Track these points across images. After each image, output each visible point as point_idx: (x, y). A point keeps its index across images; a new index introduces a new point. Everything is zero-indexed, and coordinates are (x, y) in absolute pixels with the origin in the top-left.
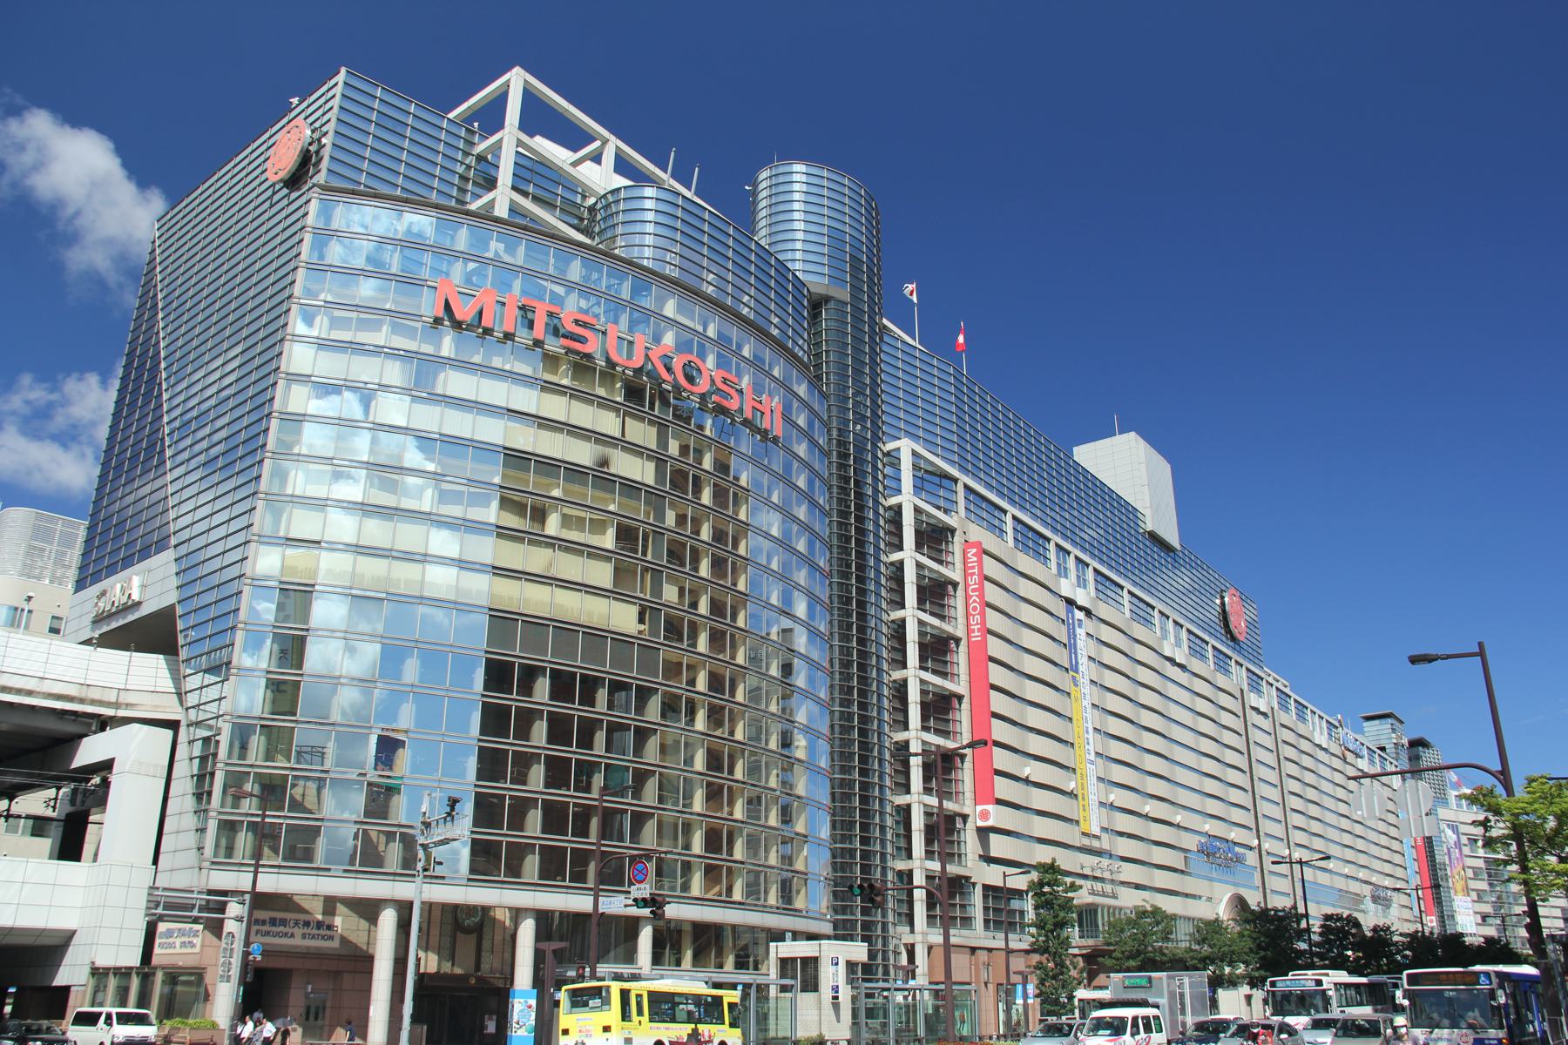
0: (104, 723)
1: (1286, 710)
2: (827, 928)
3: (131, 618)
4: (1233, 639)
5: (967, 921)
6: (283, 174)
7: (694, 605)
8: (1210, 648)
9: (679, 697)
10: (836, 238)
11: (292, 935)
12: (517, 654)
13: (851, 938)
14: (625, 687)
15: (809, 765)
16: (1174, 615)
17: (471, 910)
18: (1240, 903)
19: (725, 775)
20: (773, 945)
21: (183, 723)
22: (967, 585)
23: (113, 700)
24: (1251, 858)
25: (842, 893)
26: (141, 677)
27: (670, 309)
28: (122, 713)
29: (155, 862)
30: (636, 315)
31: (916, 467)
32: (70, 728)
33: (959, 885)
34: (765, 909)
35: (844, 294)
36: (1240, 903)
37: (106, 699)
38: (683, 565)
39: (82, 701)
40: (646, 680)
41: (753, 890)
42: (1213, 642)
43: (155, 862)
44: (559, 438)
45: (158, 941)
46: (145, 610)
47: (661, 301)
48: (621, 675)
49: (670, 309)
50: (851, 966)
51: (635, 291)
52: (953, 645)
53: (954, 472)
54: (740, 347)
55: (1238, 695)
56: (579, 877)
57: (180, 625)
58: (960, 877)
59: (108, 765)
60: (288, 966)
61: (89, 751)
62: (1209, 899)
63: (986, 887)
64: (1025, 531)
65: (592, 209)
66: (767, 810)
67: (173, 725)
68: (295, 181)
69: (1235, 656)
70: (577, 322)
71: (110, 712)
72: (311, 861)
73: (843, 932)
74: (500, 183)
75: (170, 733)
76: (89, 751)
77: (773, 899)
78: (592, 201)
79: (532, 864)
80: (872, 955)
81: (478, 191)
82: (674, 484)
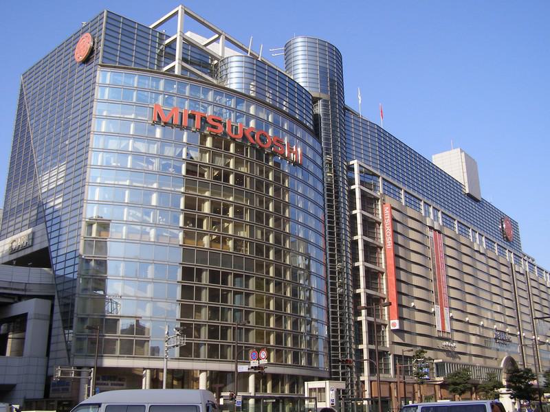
0: (20, 298)
1: (533, 272)
2: (327, 375)
3: (28, 251)
4: (508, 240)
5: (387, 371)
6: (81, 58)
7: (268, 239)
8: (496, 245)
9: (263, 279)
10: (323, 71)
11: (108, 385)
12: (195, 265)
13: (337, 379)
14: (241, 276)
15: (318, 306)
16: (479, 231)
17: (179, 371)
18: (511, 361)
19: (283, 311)
20: (306, 383)
21: (56, 297)
22: (384, 226)
23: (23, 288)
24: (515, 340)
25: (333, 362)
26: (33, 276)
27: (252, 110)
28: (27, 293)
29: (48, 354)
30: (238, 114)
31: (361, 172)
32: (11, 301)
33: (384, 354)
34: (287, 365)
35: (325, 96)
36: (511, 361)
37: (20, 288)
38: (263, 223)
39: (11, 289)
40: (249, 273)
41: (296, 358)
42: (497, 242)
43: (48, 354)
44: (110, 58)
45: (51, 388)
46: (36, 248)
47: (248, 107)
48: (238, 271)
49: (252, 110)
50: (338, 391)
51: (237, 104)
52: (379, 250)
53: (378, 173)
54: (283, 125)
55: (510, 266)
56: (224, 356)
57: (54, 255)
58: (384, 351)
59: (26, 315)
60: (312, 375)
61: (18, 308)
62: (496, 359)
63: (395, 356)
64: (410, 197)
65: (216, 66)
66: (286, 322)
67: (51, 298)
68: (87, 60)
69: (508, 248)
70: (213, 119)
71: (23, 293)
72: (226, 358)
73: (333, 377)
74: (177, 57)
75: (48, 302)
76: (18, 308)
77: (304, 362)
78: (216, 62)
79: (204, 351)
80: (347, 386)
81: (167, 61)
82: (258, 188)
